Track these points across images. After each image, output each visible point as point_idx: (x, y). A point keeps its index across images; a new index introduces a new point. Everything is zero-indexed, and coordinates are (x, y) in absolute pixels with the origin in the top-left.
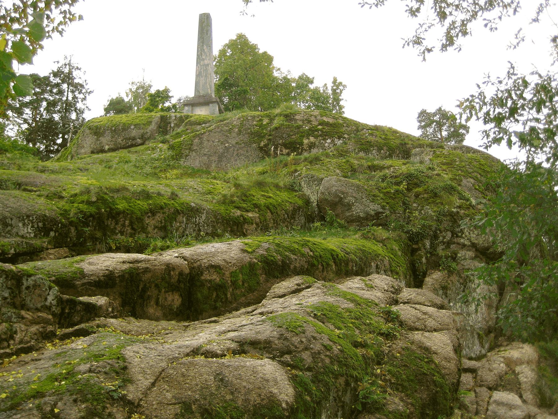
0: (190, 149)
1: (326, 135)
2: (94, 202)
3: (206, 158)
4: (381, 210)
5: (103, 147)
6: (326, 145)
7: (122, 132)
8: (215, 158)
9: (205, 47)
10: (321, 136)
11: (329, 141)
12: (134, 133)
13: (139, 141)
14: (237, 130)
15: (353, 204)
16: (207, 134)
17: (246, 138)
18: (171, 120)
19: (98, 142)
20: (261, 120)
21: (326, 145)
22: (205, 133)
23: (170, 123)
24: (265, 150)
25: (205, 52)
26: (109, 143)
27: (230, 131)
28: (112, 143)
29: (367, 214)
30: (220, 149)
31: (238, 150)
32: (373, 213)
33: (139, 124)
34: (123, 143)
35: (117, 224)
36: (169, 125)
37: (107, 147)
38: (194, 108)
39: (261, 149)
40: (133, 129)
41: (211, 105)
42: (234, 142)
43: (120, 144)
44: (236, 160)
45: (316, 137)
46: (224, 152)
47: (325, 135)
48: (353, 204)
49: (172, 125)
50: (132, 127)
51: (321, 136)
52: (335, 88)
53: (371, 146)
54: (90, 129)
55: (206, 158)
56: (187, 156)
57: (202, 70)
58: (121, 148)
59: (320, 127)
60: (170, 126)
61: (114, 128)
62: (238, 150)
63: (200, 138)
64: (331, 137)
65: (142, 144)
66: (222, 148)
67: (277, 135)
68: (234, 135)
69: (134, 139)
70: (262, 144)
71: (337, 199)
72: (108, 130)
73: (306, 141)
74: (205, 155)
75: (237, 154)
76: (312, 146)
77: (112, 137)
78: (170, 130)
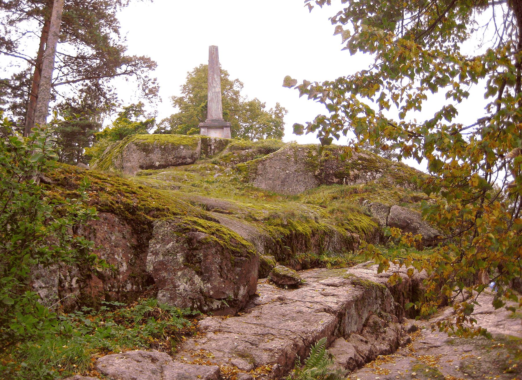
0: (256, 173)
1: (366, 169)
2: (286, 225)
3: (271, 182)
4: (439, 234)
5: (153, 163)
6: (368, 177)
7: (172, 150)
8: (278, 182)
9: (215, 76)
10: (362, 169)
11: (369, 174)
12: (184, 153)
13: (189, 160)
14: (293, 159)
15: (418, 228)
16: (269, 161)
17: (302, 167)
18: (211, 143)
19: (148, 158)
20: (309, 152)
21: (368, 177)
22: (266, 160)
23: (210, 145)
24: (319, 178)
25: (215, 81)
26: (160, 160)
27: (288, 159)
28: (163, 160)
29: (429, 236)
30: (283, 175)
31: (297, 177)
32: (433, 236)
33: (187, 145)
34: (173, 161)
35: (298, 243)
36: (209, 147)
37: (157, 164)
38: (209, 130)
39: (316, 177)
40: (183, 149)
41: (225, 129)
42: (293, 170)
43: (171, 161)
44: (296, 185)
45: (359, 170)
46: (286, 178)
47: (365, 169)
48: (418, 228)
49: (213, 147)
50: (182, 147)
51: (362, 169)
52: (277, 112)
53: (403, 180)
54: (137, 145)
55: (271, 182)
56: (254, 179)
57: (214, 97)
58: (172, 165)
59: (359, 161)
60: (211, 148)
61: (163, 147)
62: (297, 177)
63: (263, 164)
64: (371, 171)
65: (192, 163)
66: (284, 174)
67: (327, 166)
68: (292, 163)
69: (184, 158)
70: (317, 173)
71: (405, 224)
72: (157, 148)
73: (351, 173)
74: (270, 179)
75: (297, 180)
76: (356, 177)
77: (162, 155)
78: (211, 151)
